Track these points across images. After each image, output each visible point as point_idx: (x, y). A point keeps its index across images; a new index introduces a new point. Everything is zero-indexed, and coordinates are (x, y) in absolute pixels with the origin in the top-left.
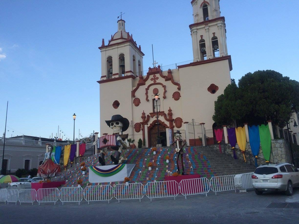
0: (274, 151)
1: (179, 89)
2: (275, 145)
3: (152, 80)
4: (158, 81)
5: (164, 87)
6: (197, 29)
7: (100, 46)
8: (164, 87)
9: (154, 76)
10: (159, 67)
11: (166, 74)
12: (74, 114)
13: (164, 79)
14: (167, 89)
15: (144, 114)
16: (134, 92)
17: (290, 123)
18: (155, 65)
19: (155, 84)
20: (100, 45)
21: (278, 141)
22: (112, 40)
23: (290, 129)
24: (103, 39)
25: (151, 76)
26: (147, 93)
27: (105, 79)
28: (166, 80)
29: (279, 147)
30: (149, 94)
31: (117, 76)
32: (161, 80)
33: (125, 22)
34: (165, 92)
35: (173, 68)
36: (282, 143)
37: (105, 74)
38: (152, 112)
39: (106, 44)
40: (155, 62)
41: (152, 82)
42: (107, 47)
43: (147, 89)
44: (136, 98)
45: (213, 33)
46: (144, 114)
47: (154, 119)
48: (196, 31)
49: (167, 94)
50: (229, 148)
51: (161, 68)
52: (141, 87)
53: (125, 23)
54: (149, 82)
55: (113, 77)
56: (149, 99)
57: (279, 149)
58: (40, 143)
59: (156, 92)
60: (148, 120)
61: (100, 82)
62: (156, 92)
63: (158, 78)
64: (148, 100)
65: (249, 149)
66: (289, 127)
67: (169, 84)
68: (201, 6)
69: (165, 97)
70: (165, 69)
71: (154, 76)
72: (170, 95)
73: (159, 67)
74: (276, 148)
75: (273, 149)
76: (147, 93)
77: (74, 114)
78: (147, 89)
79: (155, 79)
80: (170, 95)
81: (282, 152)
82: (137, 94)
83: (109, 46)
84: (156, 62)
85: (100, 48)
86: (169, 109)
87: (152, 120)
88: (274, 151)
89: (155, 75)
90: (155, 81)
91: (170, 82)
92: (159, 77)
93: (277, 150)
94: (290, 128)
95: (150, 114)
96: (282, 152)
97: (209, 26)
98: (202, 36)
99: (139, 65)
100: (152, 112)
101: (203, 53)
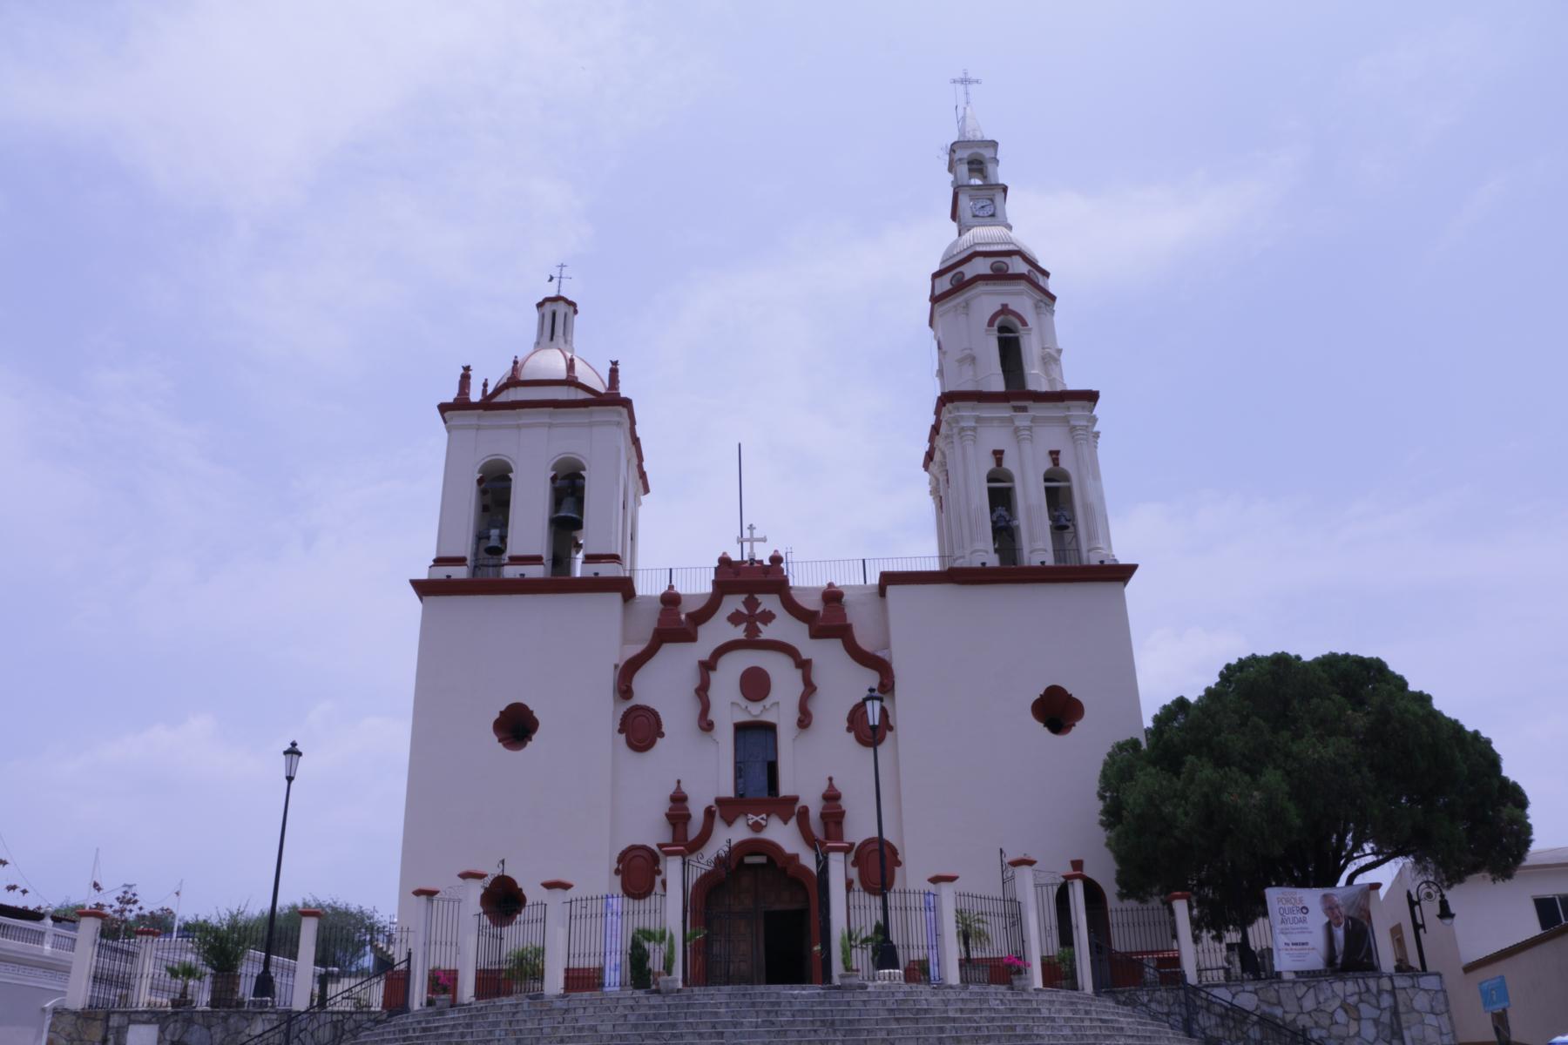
0: (1409, 1028)
1: (886, 686)
2: (1411, 1000)
3: (735, 619)
4: (767, 632)
5: (804, 665)
6: (978, 419)
7: (450, 399)
8: (804, 665)
9: (751, 604)
10: (776, 560)
11: (813, 604)
12: (294, 744)
13: (803, 628)
14: (816, 678)
15: (679, 799)
16: (629, 670)
17: (1422, 902)
18: (752, 547)
19: (752, 642)
20: (450, 395)
21: (1421, 979)
22: (513, 381)
23: (1424, 928)
24: (467, 369)
25: (734, 603)
26: (702, 690)
27: (460, 573)
28: (817, 634)
29: (1428, 1008)
30: (713, 694)
31: (535, 572)
32: (783, 628)
33: (576, 312)
34: (810, 687)
35: (847, 578)
36: (1437, 992)
37: (463, 546)
38: (728, 791)
39: (475, 395)
40: (752, 534)
41: (739, 633)
42: (475, 406)
43: (707, 666)
44: (637, 708)
45: (1051, 453)
46: (679, 799)
47: (739, 832)
48: (973, 424)
49: (818, 706)
50: (1208, 1010)
51: (783, 565)
52: (669, 651)
53: (576, 317)
54: (718, 631)
55: (511, 572)
56: (712, 716)
57: (1430, 1019)
58: (739, 781)
59: (755, 685)
60: (706, 834)
61: (423, 588)
62: (755, 685)
63: (768, 617)
64: (706, 725)
65: (1300, 1017)
66: (1419, 921)
67: (828, 656)
68: (991, 323)
69: (804, 721)
70: (805, 577)
71: (751, 604)
72: (833, 707)
73: (776, 560)
74: (1416, 1015)
75: (1403, 1018)
76: (702, 690)
77: (294, 744)
78: (707, 666)
79: (752, 618)
80: (833, 707)
81: (1441, 1034)
82: (647, 689)
83: (489, 403)
84: (757, 534)
85: (443, 408)
86: (824, 786)
87: (727, 837)
88: (1409, 1028)
89: (757, 596)
90: (752, 631)
91: (835, 647)
92: (774, 612)
93: (1422, 1022)
94: (1423, 926)
95: (720, 802)
96: (1441, 1034)
97: (1034, 419)
98: (998, 455)
99: (632, 539)
100: (728, 791)
101: (1005, 534)
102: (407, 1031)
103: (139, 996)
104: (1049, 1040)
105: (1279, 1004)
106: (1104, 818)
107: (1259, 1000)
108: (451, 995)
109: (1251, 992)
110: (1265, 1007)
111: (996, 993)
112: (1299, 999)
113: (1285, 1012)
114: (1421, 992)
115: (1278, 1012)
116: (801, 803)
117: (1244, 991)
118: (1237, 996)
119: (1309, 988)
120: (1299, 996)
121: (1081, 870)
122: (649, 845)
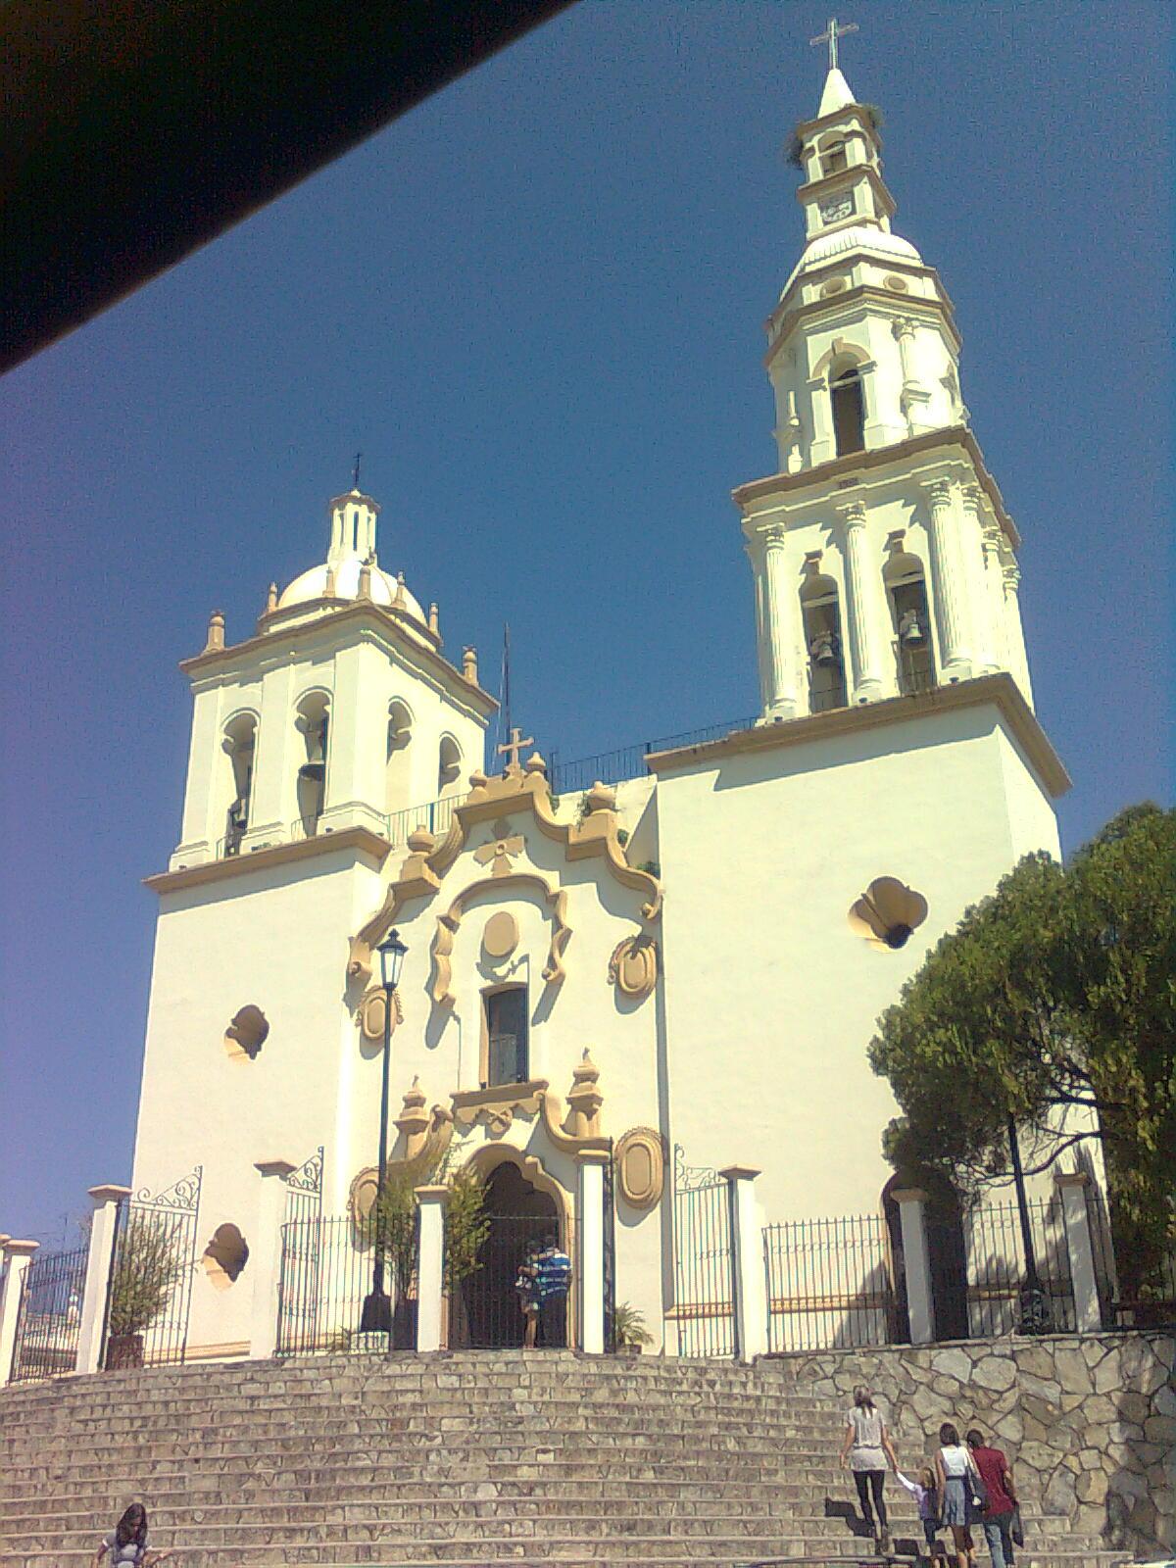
102: (343, 1425)
103: (289, 1330)
104: (289, 1521)
105: (1054, 1378)
106: (1057, 857)
107: (1018, 1370)
108: (1131, 1323)
109: (1004, 1356)
110: (1028, 1385)
111: (474, 1364)
112: (1090, 1369)
113: (1064, 1392)
114: (1096, 1370)
115: (1052, 1392)
116: (1035, 852)
117: (992, 1355)
118: (980, 1364)
119: (1110, 1350)
120: (1091, 1364)
121: (441, 877)
122: (526, 857)
